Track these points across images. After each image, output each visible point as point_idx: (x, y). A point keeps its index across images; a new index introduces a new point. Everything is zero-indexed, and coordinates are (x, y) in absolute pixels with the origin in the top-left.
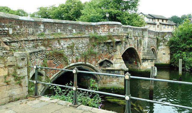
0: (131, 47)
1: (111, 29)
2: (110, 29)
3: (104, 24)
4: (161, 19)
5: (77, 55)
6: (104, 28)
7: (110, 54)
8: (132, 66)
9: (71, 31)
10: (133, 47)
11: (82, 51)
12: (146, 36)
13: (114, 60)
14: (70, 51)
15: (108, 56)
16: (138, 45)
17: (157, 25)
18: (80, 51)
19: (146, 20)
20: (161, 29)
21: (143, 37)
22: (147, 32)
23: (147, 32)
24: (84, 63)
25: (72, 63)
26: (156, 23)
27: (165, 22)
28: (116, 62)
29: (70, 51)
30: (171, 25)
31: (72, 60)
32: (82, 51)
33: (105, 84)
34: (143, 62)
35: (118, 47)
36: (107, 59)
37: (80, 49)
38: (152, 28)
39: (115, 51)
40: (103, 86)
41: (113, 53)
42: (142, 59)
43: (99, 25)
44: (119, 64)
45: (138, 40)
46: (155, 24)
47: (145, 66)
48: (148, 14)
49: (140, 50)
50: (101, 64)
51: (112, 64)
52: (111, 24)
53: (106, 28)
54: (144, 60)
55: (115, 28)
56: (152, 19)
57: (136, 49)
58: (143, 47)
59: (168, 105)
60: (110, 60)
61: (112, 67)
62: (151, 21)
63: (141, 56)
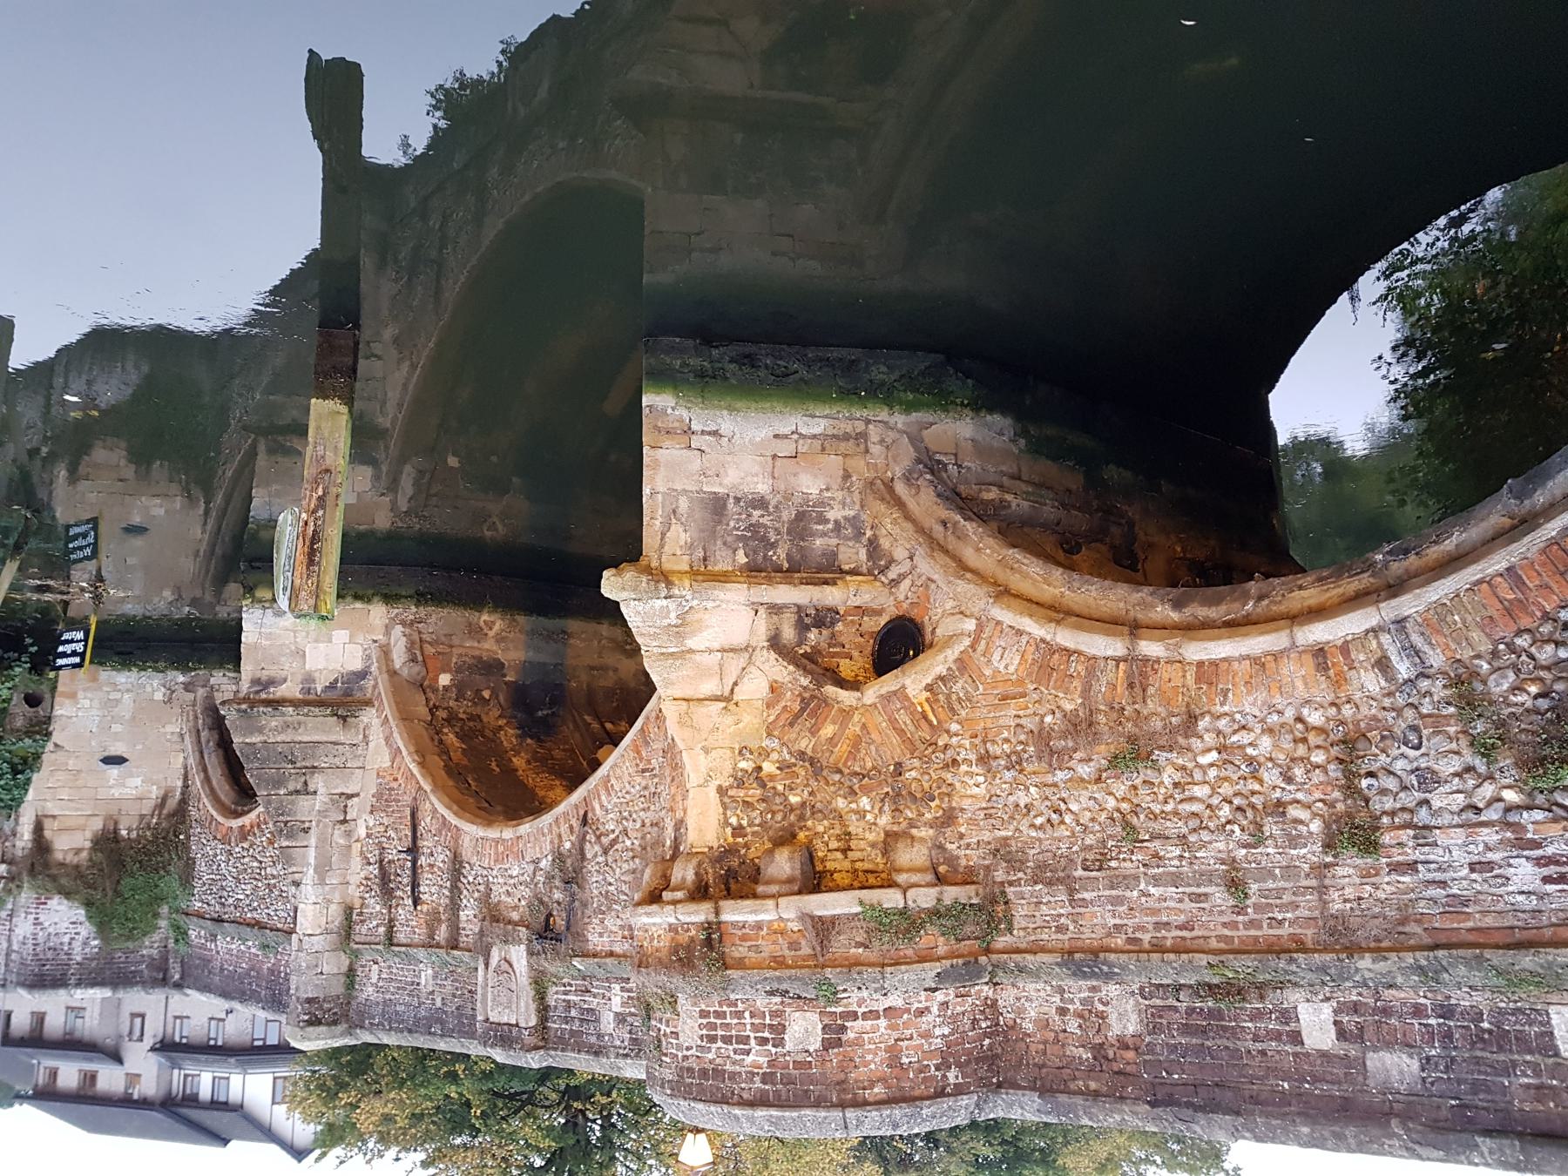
1: (815, 1044)
2: (827, 1045)
3: (897, 1112)
5: (1266, 743)
7: (802, 755)
9: (1364, 1026)
10: (472, 831)
11: (1201, 791)
12: (318, 943)
13: (754, 687)
14: (1391, 783)
15: (828, 730)
16: (413, 850)
17: (148, 1042)
18: (1227, 789)
19: (254, 1088)
21: (346, 932)
22: (302, 986)
23: (302, 986)
24: (1151, 648)
25: (1345, 649)
26: (154, 1059)
28: (734, 664)
29: (1391, 783)
31: (1339, 682)
32: (1201, 791)
33: (846, 437)
34: (363, 674)
35: (705, 826)
36: (846, 697)
37: (1225, 812)
39: (740, 784)
41: (769, 767)
42: (368, 703)
43: (959, 1090)
46: (167, 1047)
48: (233, 1144)
51: (775, 643)
52: (817, 1105)
53: (875, 1063)
54: (342, 701)
55: (757, 1057)
56: (192, 1100)
57: (436, 808)
58: (348, 834)
60: (805, 681)
61: (775, 609)
62: (205, 1081)
63: (379, 750)
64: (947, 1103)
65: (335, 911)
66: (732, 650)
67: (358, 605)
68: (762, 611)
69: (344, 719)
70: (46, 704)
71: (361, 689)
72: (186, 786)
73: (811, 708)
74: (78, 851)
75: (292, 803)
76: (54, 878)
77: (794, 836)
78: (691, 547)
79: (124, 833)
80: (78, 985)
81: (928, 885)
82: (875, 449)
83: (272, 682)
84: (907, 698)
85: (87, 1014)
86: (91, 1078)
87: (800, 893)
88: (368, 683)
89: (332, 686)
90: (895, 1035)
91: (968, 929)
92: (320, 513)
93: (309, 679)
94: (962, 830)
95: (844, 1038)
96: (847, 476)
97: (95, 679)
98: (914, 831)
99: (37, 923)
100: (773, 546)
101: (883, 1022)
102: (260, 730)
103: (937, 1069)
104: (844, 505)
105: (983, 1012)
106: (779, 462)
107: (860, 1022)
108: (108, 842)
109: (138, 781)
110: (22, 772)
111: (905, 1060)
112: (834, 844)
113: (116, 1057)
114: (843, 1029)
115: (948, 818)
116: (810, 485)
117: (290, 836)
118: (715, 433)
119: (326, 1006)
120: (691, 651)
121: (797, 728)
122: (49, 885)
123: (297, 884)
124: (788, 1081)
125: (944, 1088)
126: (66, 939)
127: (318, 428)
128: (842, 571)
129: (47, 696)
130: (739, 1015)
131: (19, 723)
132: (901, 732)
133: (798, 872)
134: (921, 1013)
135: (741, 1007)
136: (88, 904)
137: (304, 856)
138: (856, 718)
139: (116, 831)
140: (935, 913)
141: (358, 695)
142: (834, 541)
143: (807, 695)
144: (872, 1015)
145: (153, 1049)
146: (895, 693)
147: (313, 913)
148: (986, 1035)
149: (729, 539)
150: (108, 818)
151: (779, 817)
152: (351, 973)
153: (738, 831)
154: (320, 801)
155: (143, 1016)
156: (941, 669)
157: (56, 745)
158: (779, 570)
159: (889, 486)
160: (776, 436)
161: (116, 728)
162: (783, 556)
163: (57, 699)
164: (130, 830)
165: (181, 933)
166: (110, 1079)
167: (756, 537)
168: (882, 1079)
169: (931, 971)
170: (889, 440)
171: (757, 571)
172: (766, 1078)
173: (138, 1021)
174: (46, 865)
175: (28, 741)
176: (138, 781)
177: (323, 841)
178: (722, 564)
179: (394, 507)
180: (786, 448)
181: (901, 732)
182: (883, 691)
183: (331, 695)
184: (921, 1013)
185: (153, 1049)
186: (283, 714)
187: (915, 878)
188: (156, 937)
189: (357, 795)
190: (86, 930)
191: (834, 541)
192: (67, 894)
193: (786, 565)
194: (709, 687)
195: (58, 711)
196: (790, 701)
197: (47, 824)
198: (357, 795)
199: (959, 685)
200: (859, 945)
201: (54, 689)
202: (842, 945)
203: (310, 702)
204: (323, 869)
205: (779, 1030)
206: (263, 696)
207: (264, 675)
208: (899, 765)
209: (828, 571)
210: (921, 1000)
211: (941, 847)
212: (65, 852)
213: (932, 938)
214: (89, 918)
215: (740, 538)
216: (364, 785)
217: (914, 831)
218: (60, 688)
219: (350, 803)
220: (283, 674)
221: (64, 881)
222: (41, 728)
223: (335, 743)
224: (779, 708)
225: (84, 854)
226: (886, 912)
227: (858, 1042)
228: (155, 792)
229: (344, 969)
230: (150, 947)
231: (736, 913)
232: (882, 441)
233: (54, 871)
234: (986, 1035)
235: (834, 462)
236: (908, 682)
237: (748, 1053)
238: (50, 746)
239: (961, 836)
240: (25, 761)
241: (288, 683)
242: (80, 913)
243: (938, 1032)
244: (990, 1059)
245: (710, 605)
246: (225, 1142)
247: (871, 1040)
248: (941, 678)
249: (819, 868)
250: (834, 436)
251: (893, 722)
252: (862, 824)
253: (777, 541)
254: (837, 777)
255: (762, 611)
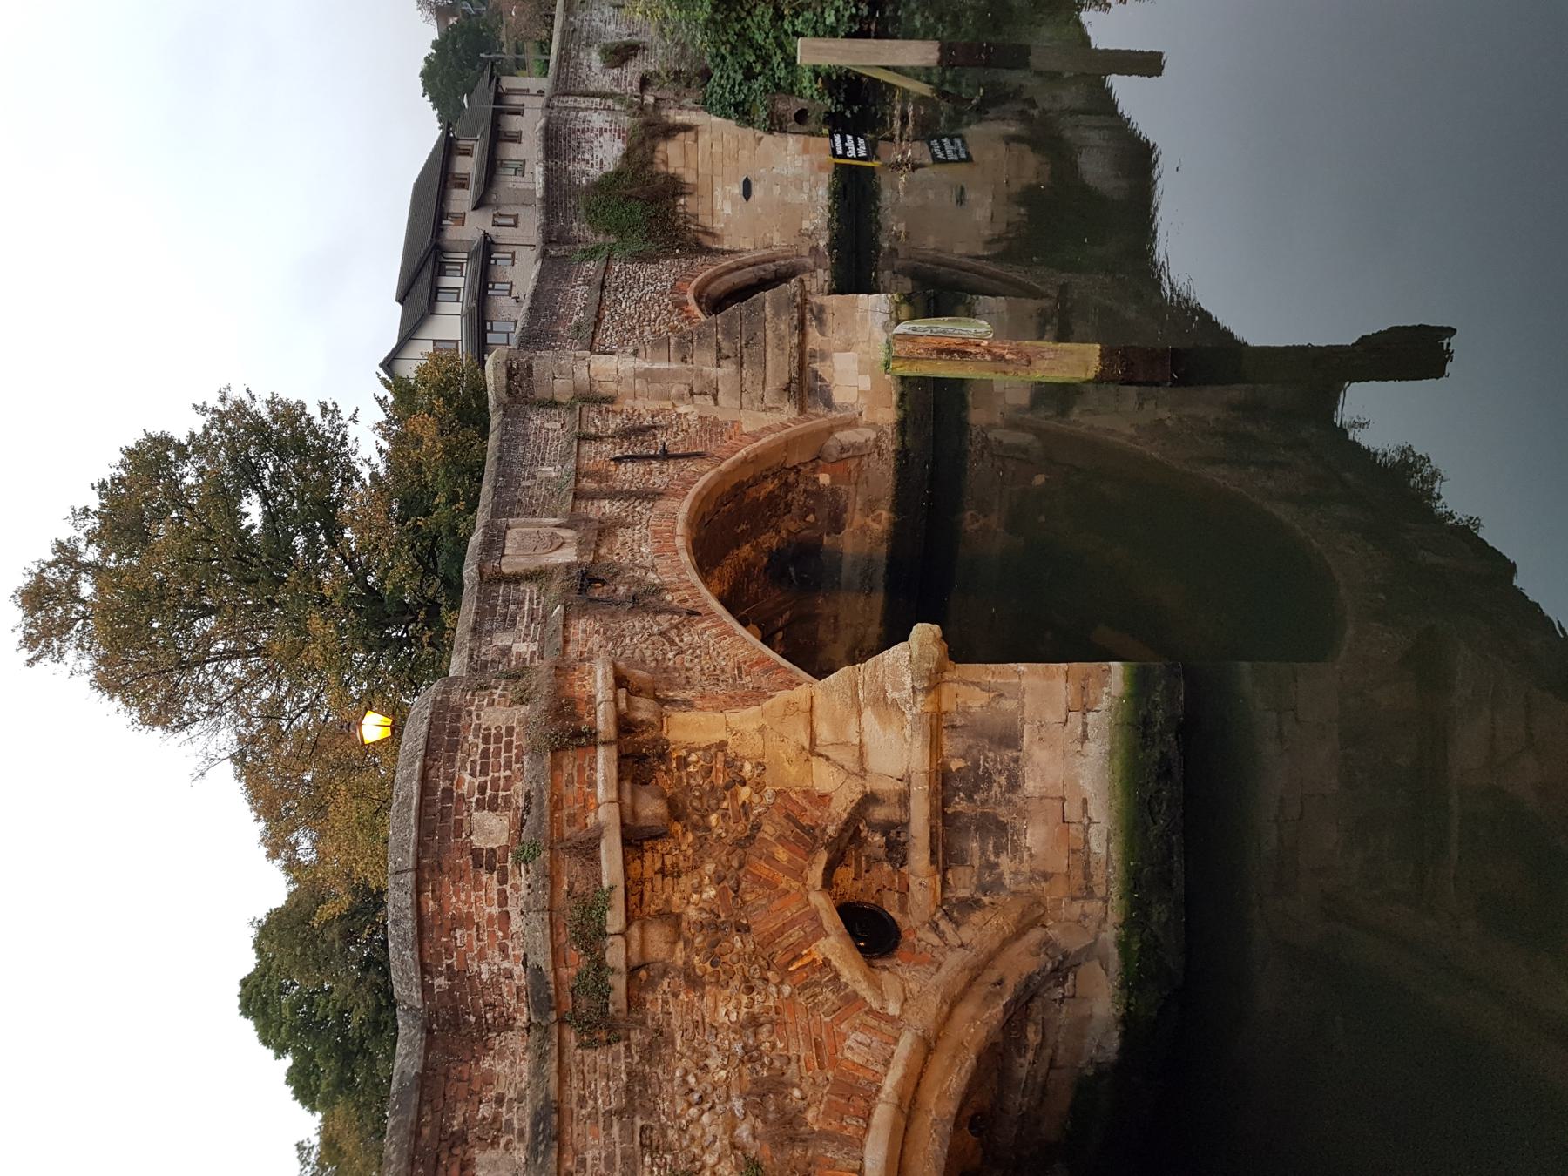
0: (680, 542)
1: (478, 841)
2: (476, 853)
4: (443, 197)
6: (464, 921)
8: (870, 507)
12: (582, 374)
13: (824, 778)
15: (782, 855)
16: (665, 456)
19: (449, 324)
20: (525, 200)
21: (593, 398)
22: (543, 362)
23: (543, 362)
26: (478, 236)
27: (467, 165)
28: (848, 758)
30: (497, 115)
33: (1087, 876)
34: (829, 404)
36: (816, 874)
38: (521, 273)
39: (729, 764)
40: (1115, 897)
41: (745, 792)
43: (427, 989)
44: (871, 723)
45: (618, 460)
46: (488, 247)
47: (865, 383)
48: (399, 307)
49: (711, 427)
50: (873, 932)
51: (870, 799)
52: (420, 843)
53: (457, 902)
54: (804, 386)
56: (440, 270)
57: (704, 476)
58: (681, 397)
59: (896, 70)
60: (831, 830)
61: (904, 799)
63: (757, 421)
64: (415, 976)
65: (612, 387)
66: (861, 755)
67: (895, 397)
68: (902, 785)
69: (787, 389)
70: (798, 128)
71: (815, 404)
72: (723, 252)
73: (805, 836)
74: (666, 163)
75: (709, 347)
76: (642, 143)
77: (677, 820)
78: (965, 712)
79: (682, 201)
80: (547, 168)
81: (628, 959)
82: (1076, 908)
83: (821, 322)
84: (816, 939)
85: (518, 178)
86: (462, 183)
87: (623, 825)
88: (821, 410)
89: (817, 377)
90: (483, 923)
91: (583, 1001)
92: (988, 358)
93: (824, 356)
94: (682, 996)
95: (482, 871)
96: (1046, 876)
97: (821, 168)
98: (681, 945)
99: (602, 131)
100: (970, 798)
101: (495, 910)
102: (776, 315)
103: (449, 967)
104: (1015, 873)
105: (501, 1015)
106: (1057, 804)
107: (496, 886)
108: (675, 187)
109: (728, 210)
110: (736, 111)
111: (458, 933)
112: (669, 860)
113: (479, 204)
114: (491, 870)
115: (694, 982)
116: (1035, 837)
117: (679, 345)
118: (1085, 737)
119: (524, 384)
120: (860, 713)
121: (784, 822)
122: (635, 139)
123: (635, 353)
124: (444, 814)
125: (430, 973)
126: (587, 156)
127: (1072, 352)
128: (945, 870)
129: (805, 129)
130: (508, 766)
131: (781, 106)
132: (781, 931)
133: (642, 823)
134: (503, 949)
135: (516, 766)
136: (618, 174)
137: (660, 359)
138: (795, 884)
139: (683, 194)
140: (600, 966)
141: (809, 401)
142: (976, 862)
143: (817, 832)
144: (503, 901)
145: (486, 234)
146: (821, 925)
147: (609, 368)
148: (479, 1018)
149: (975, 752)
150: (695, 187)
151: (696, 803)
152: (553, 404)
153: (683, 763)
154: (711, 371)
155: (515, 225)
156: (846, 976)
157: (760, 139)
158: (945, 803)
159: (1038, 922)
160: (1085, 801)
161: (777, 190)
162: (959, 808)
163: (802, 137)
164: (684, 206)
165: (592, 254)
166: (461, 200)
167: (978, 780)
168: (441, 909)
169: (543, 960)
170: (1086, 923)
171: (943, 782)
172: (448, 792)
173: (511, 221)
174: (653, 136)
175: (764, 115)
176: (728, 210)
177: (673, 376)
178: (949, 745)
179: (992, 426)
180: (1073, 811)
181: (781, 931)
182: (822, 913)
183: (809, 376)
184: (503, 949)
185: (486, 234)
186: (791, 335)
187: (635, 945)
188: (588, 234)
189: (716, 404)
190: (595, 172)
191: (976, 862)
192: (627, 156)
193: (950, 811)
194: (824, 732)
195: (791, 139)
196: (812, 814)
197: (691, 135)
198: (716, 404)
199: (830, 996)
200: (571, 885)
201: (812, 134)
202: (571, 869)
203: (803, 358)
204: (648, 376)
205: (492, 806)
206: (808, 316)
207: (828, 316)
208: (748, 929)
209: (945, 856)
210: (515, 950)
211: (665, 973)
212: (665, 152)
213: (576, 962)
214: (606, 175)
215: (976, 765)
216: (726, 409)
217: (681, 945)
218: (812, 139)
219: (709, 397)
220: (829, 333)
221: (639, 152)
222: (776, 125)
223: (764, 382)
224: (804, 803)
225: (663, 168)
226: (602, 914)
227: (478, 885)
228: (718, 226)
229: (557, 398)
230: (580, 229)
231: (604, 762)
232: (1085, 915)
233: (648, 144)
234: (479, 1018)
235: (1061, 863)
236: (832, 940)
237: (472, 774)
238: (760, 133)
239: (676, 995)
240: (747, 113)
241: (820, 338)
242: (610, 167)
243: (484, 967)
244: (456, 1022)
245: (907, 732)
246: (401, 299)
247: (479, 899)
248: (837, 976)
249: (646, 845)
250: (1088, 863)
251: (791, 923)
252: (689, 890)
253: (974, 801)
254: (735, 864)
255: (902, 785)
